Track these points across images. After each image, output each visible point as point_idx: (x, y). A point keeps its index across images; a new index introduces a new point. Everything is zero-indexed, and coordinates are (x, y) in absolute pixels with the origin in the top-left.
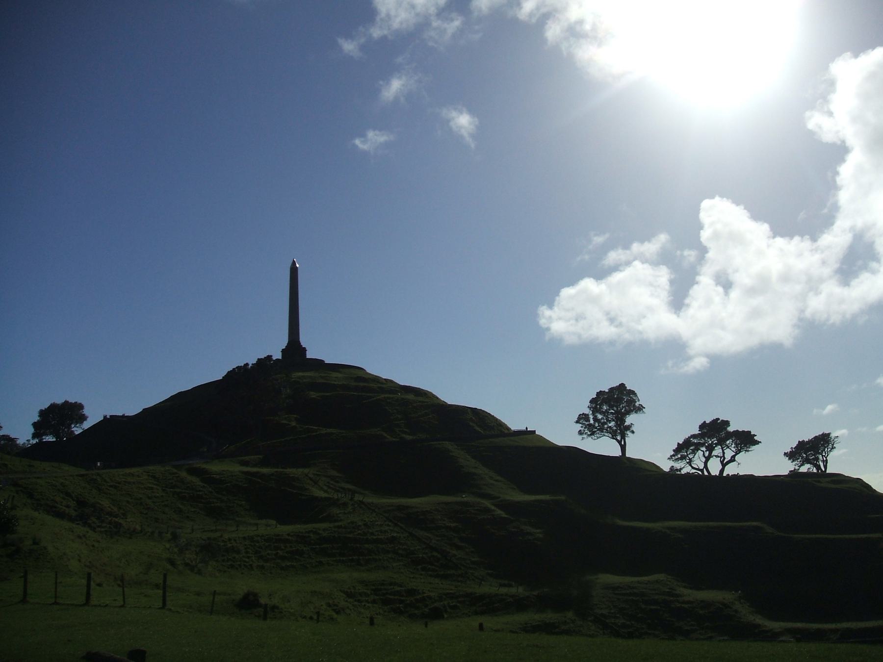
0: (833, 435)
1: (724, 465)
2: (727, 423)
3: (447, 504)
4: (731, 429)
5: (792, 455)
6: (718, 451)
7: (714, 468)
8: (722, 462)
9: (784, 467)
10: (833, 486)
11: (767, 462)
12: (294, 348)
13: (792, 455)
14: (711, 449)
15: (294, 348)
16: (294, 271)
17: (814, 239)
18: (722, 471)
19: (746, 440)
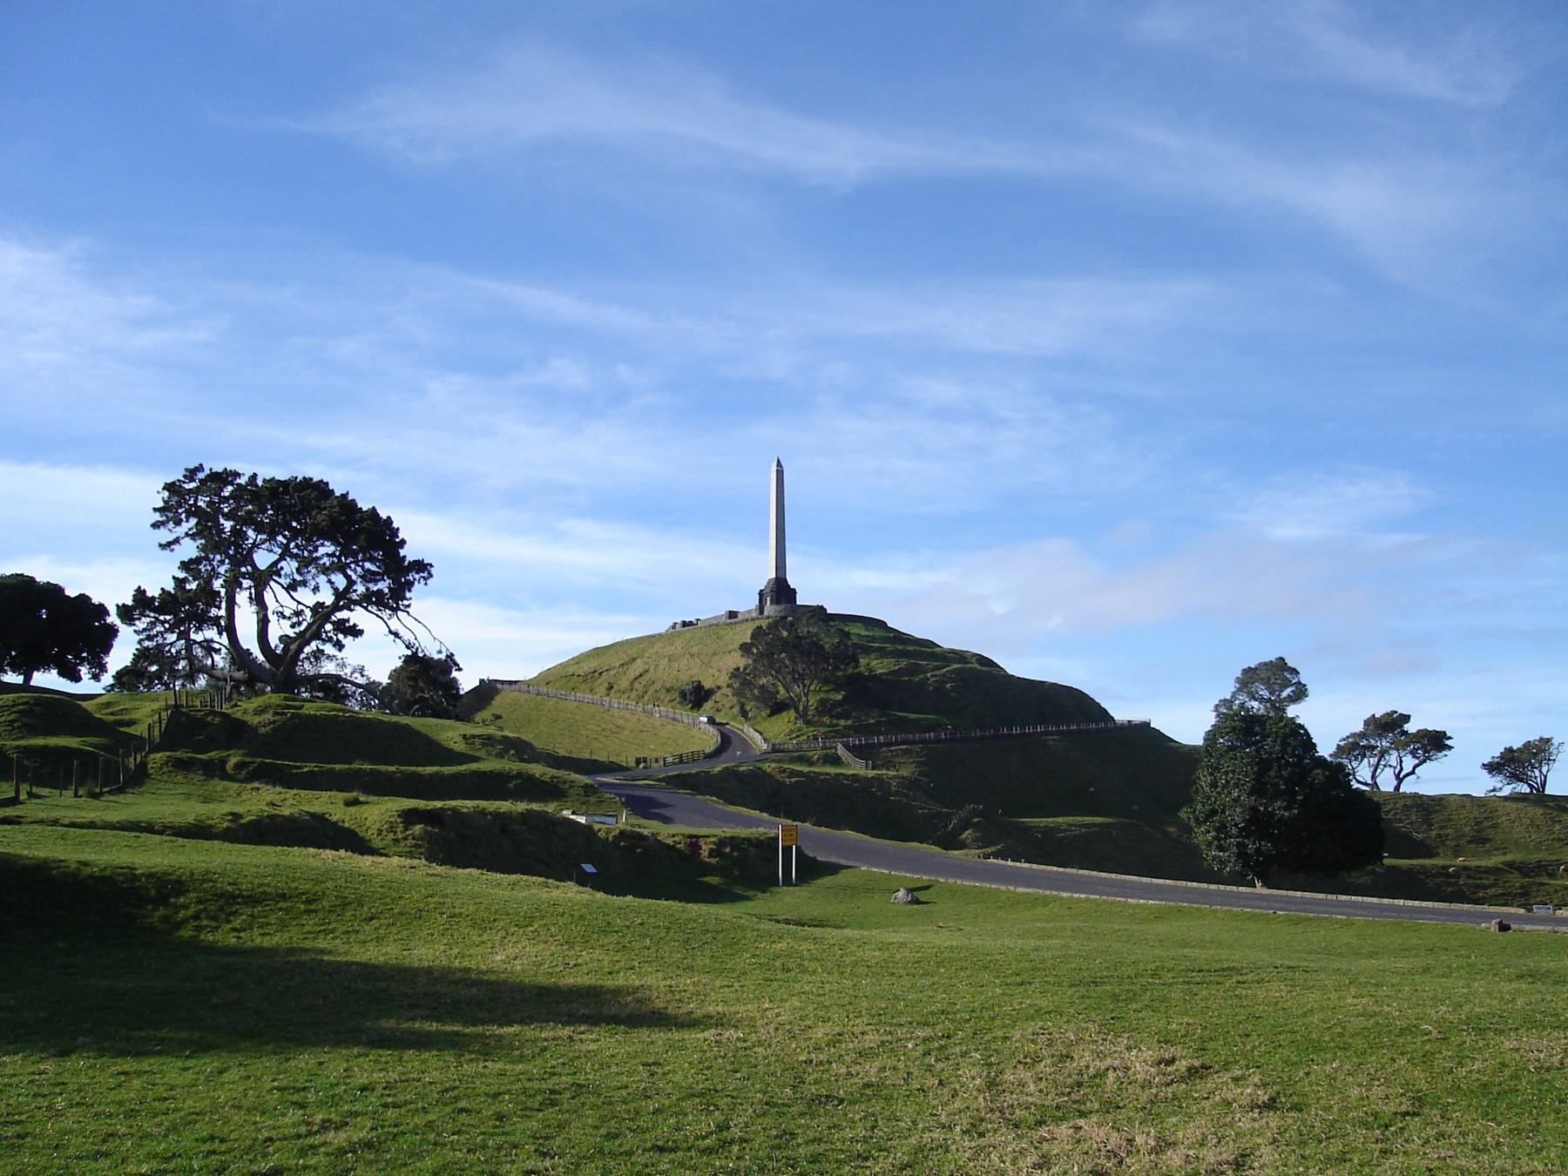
0: (1555, 742)
1: (1400, 779)
2: (1406, 718)
3: (1094, 825)
4: (1411, 727)
5: (1492, 768)
6: (1393, 758)
7: (1386, 782)
8: (1397, 776)
9: (1481, 785)
10: (329, 804)
11: (1457, 776)
12: (781, 590)
13: (1492, 768)
14: (1383, 753)
15: (781, 590)
16: (779, 464)
17: (415, 654)
18: (1397, 788)
19: (1435, 743)
